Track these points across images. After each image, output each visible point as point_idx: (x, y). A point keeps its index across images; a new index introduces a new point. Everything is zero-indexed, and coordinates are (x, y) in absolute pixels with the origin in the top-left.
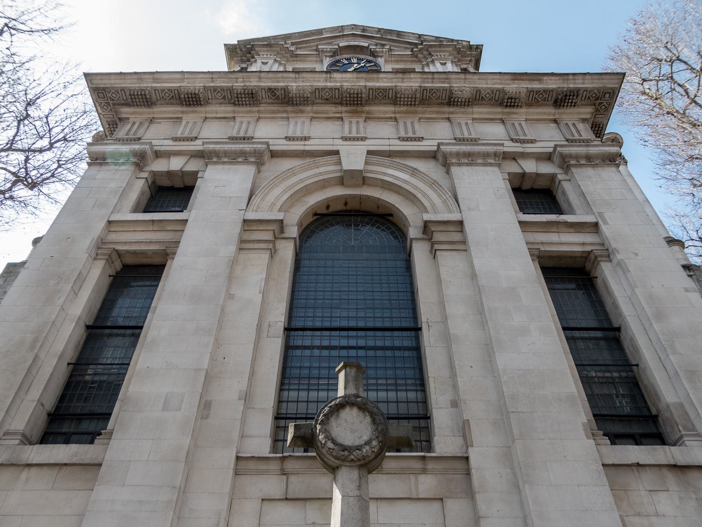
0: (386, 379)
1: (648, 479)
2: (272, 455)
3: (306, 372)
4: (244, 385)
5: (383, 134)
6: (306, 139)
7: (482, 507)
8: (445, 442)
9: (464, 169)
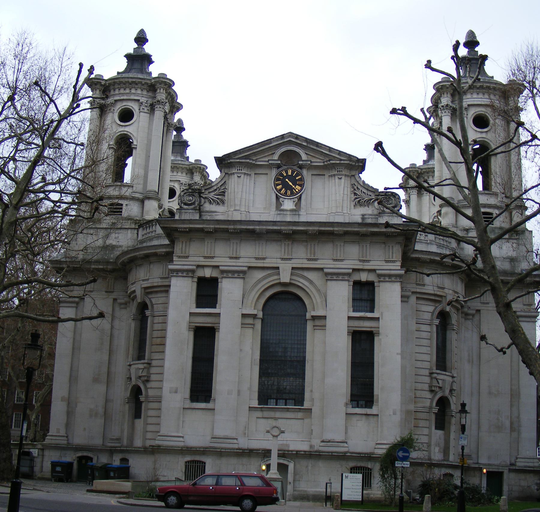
1: (358, 417)
5: (300, 255)
6: (264, 259)
8: (306, 405)
9: (334, 283)
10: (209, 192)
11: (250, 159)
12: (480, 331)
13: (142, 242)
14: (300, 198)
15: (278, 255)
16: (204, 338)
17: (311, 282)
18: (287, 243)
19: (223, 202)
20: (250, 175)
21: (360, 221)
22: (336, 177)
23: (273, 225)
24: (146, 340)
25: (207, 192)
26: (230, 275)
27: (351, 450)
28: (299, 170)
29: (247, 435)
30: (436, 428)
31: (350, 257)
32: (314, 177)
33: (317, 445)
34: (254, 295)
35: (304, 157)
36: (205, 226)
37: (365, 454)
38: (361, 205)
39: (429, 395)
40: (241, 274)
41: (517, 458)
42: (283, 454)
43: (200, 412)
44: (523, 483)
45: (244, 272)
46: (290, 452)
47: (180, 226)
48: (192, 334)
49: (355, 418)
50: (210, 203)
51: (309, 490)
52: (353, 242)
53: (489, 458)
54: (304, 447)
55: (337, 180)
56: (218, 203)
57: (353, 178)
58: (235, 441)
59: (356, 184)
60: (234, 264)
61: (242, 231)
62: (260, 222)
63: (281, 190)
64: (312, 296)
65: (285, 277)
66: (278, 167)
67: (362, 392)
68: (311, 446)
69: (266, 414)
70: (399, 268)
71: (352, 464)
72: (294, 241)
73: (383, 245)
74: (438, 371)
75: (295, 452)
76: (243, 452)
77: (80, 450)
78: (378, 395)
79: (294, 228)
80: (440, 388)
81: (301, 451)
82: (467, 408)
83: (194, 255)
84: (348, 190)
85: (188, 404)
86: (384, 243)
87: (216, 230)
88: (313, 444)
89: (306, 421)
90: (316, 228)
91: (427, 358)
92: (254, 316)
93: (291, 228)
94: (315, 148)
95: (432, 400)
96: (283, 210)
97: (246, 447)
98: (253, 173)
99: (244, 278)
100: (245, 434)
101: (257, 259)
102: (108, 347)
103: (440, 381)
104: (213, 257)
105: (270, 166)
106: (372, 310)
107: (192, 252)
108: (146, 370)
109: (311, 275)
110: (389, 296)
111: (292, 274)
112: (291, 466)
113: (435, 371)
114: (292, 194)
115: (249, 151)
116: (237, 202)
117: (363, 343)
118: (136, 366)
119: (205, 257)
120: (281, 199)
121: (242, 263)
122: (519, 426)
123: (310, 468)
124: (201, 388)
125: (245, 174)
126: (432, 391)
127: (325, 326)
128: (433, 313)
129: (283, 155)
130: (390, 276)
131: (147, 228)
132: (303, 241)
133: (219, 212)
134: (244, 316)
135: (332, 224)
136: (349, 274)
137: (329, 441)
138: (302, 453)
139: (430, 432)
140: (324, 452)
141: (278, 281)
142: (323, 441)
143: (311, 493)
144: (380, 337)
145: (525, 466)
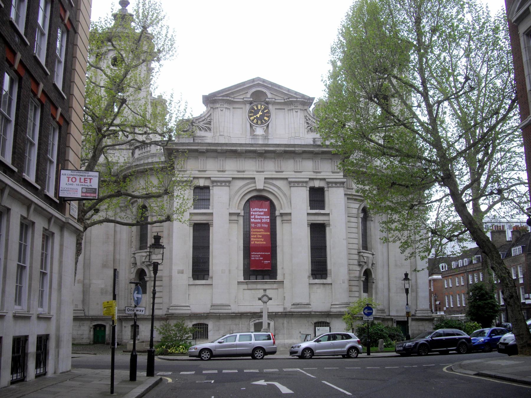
1: (318, 286)
5: (270, 167)
8: (279, 278)
10: (199, 122)
11: (230, 97)
13: (139, 159)
14: (268, 126)
15: (254, 169)
16: (201, 231)
17: (279, 188)
18: (260, 160)
19: (210, 129)
20: (229, 109)
21: (312, 143)
22: (294, 111)
23: (251, 147)
24: (147, 234)
25: (197, 121)
26: (219, 184)
27: (314, 310)
28: (266, 105)
30: (364, 292)
31: (307, 169)
32: (277, 110)
33: (289, 308)
34: (237, 198)
35: (269, 95)
36: (199, 147)
37: (325, 312)
38: (312, 131)
39: (358, 268)
40: (227, 183)
41: (416, 311)
43: (201, 287)
44: (421, 328)
45: (229, 182)
47: (180, 148)
48: (192, 228)
49: (315, 287)
50: (200, 130)
52: (309, 158)
53: (397, 311)
55: (294, 113)
56: (206, 130)
57: (305, 111)
58: (188, 308)
59: (308, 116)
60: (222, 176)
61: (227, 151)
62: (241, 145)
63: (253, 120)
64: (280, 198)
65: (260, 185)
66: (251, 103)
67: (319, 268)
68: (284, 309)
69: (250, 286)
70: (342, 177)
71: (315, 320)
72: (265, 158)
73: (330, 161)
74: (364, 251)
77: (95, 320)
78: (331, 270)
79: (266, 149)
80: (365, 262)
82: (409, 277)
83: (190, 169)
84: (303, 120)
85: (192, 281)
86: (331, 159)
87: (208, 151)
89: (280, 290)
90: (283, 149)
91: (356, 241)
92: (238, 215)
93: (264, 148)
94: (278, 89)
95: (360, 271)
96: (256, 135)
97: (237, 311)
98: (231, 107)
99: (229, 186)
100: (236, 302)
101: (238, 171)
102: (113, 241)
103: (365, 258)
104: (205, 171)
105: (244, 103)
106: (323, 208)
107: (189, 167)
108: (148, 257)
109: (278, 183)
110: (336, 199)
111: (265, 183)
113: (362, 251)
114: (262, 123)
115: (226, 91)
116: (221, 129)
117: (318, 231)
118: (140, 254)
119: (199, 171)
120: (254, 127)
121: (228, 175)
122: (417, 288)
124: (201, 269)
125: (226, 108)
126: (360, 265)
127: (291, 220)
128: (358, 209)
129: (253, 94)
130: (336, 183)
131: (142, 148)
132: (272, 158)
133: (209, 137)
134: (231, 214)
135: (294, 146)
136: (306, 182)
137: (298, 305)
139: (360, 294)
141: (254, 188)
142: (294, 305)
144: (331, 227)
145: (423, 316)
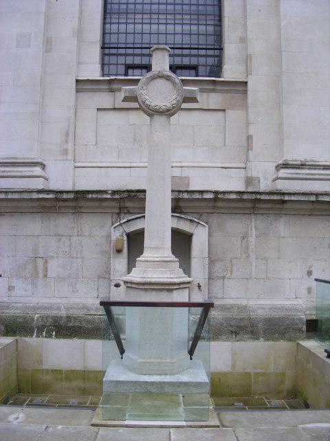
0: (190, 14)
2: (102, 78)
3: (124, 7)
4: (75, 24)
7: (252, 117)
8: (230, 72)
12: (247, 132)
29: (70, 157)
33: (266, 179)
42: (182, 203)
46: (197, 196)
51: (252, 303)
54: (231, 183)
58: (37, 171)
68: (249, 181)
75: (211, 196)
76: (57, 199)
81: (231, 192)
88: (255, 174)
100: (66, 152)
112: (200, 237)
123: (252, 240)
137: (302, 166)
138: (233, 196)
140: (290, 194)
142: (286, 166)
143: (260, 313)
